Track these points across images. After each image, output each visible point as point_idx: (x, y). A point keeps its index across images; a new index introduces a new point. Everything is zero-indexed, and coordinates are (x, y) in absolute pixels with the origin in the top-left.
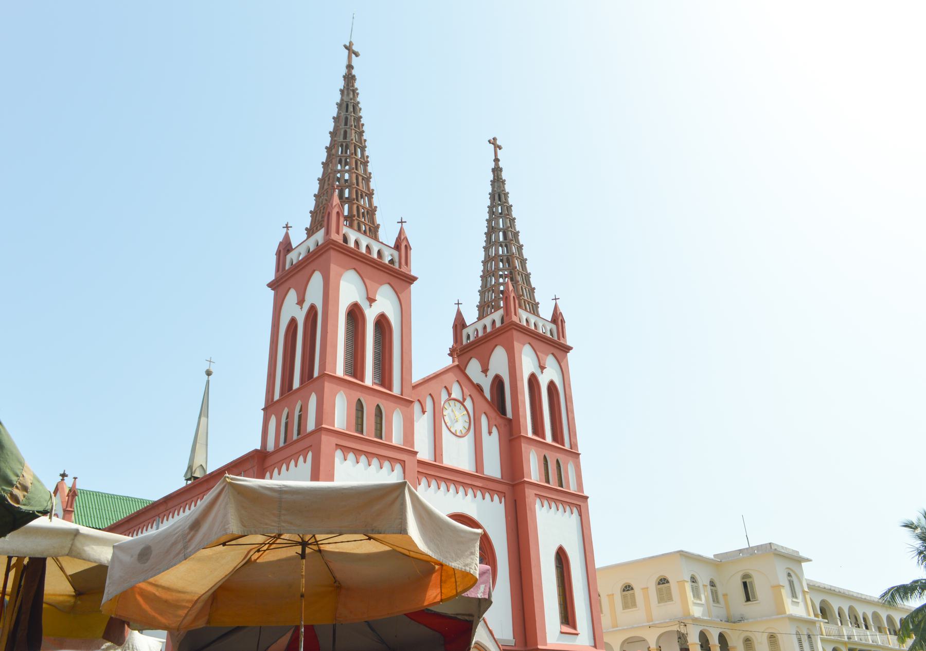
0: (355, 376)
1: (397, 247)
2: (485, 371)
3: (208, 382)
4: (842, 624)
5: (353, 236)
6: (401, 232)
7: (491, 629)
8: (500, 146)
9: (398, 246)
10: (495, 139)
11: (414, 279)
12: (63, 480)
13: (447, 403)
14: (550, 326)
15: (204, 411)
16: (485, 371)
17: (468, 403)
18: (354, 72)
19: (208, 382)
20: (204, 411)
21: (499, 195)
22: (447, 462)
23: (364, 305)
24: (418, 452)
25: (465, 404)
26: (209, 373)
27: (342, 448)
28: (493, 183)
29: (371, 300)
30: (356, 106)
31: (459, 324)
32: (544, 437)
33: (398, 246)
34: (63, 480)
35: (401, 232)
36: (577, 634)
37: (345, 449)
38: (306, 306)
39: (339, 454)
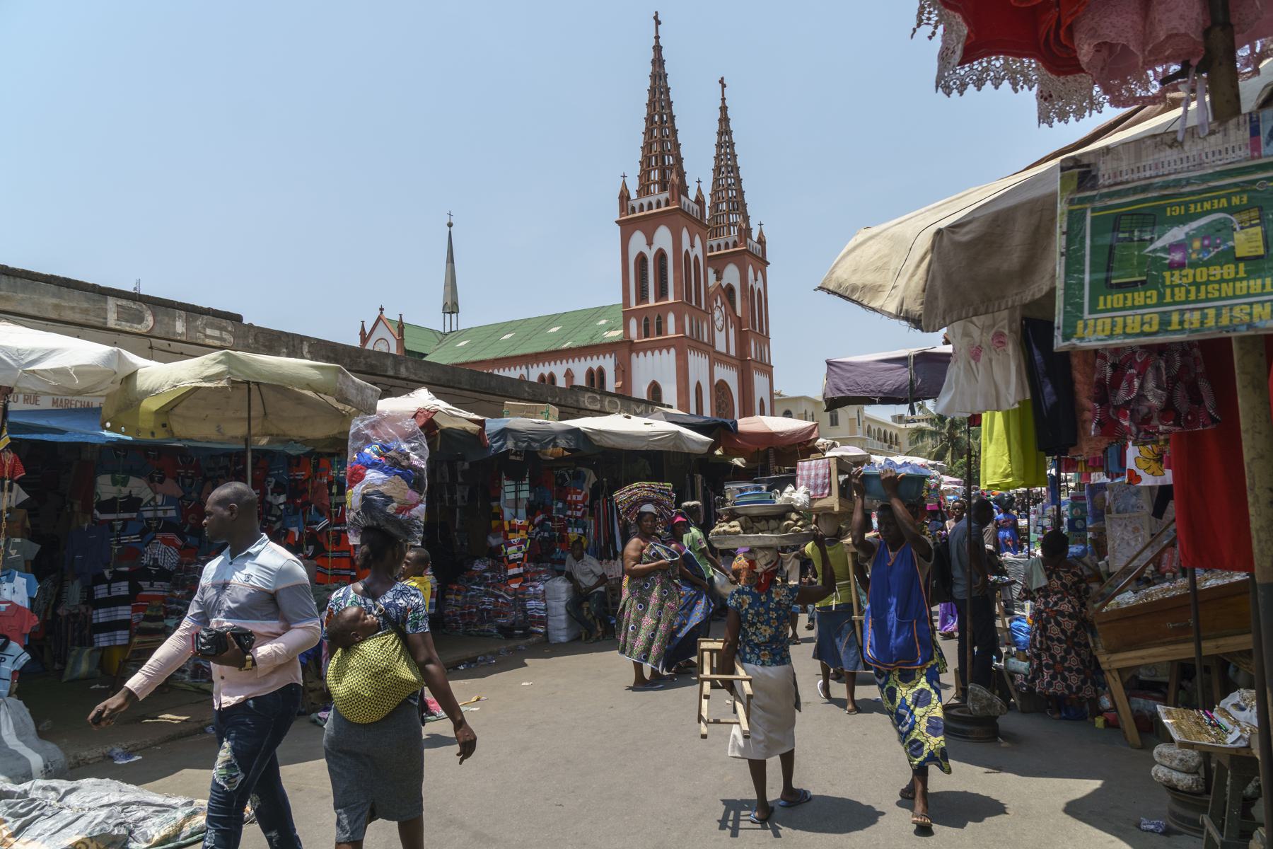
2: (650, 243)
3: (450, 232)
4: (318, 571)
10: (722, 79)
12: (382, 313)
14: (696, 207)
15: (451, 259)
16: (650, 243)
17: (723, 309)
18: (661, 44)
19: (450, 232)
20: (451, 259)
21: (658, 62)
26: (450, 225)
28: (720, 121)
30: (732, 145)
31: (624, 197)
32: (691, 302)
34: (382, 313)
38: (655, 248)
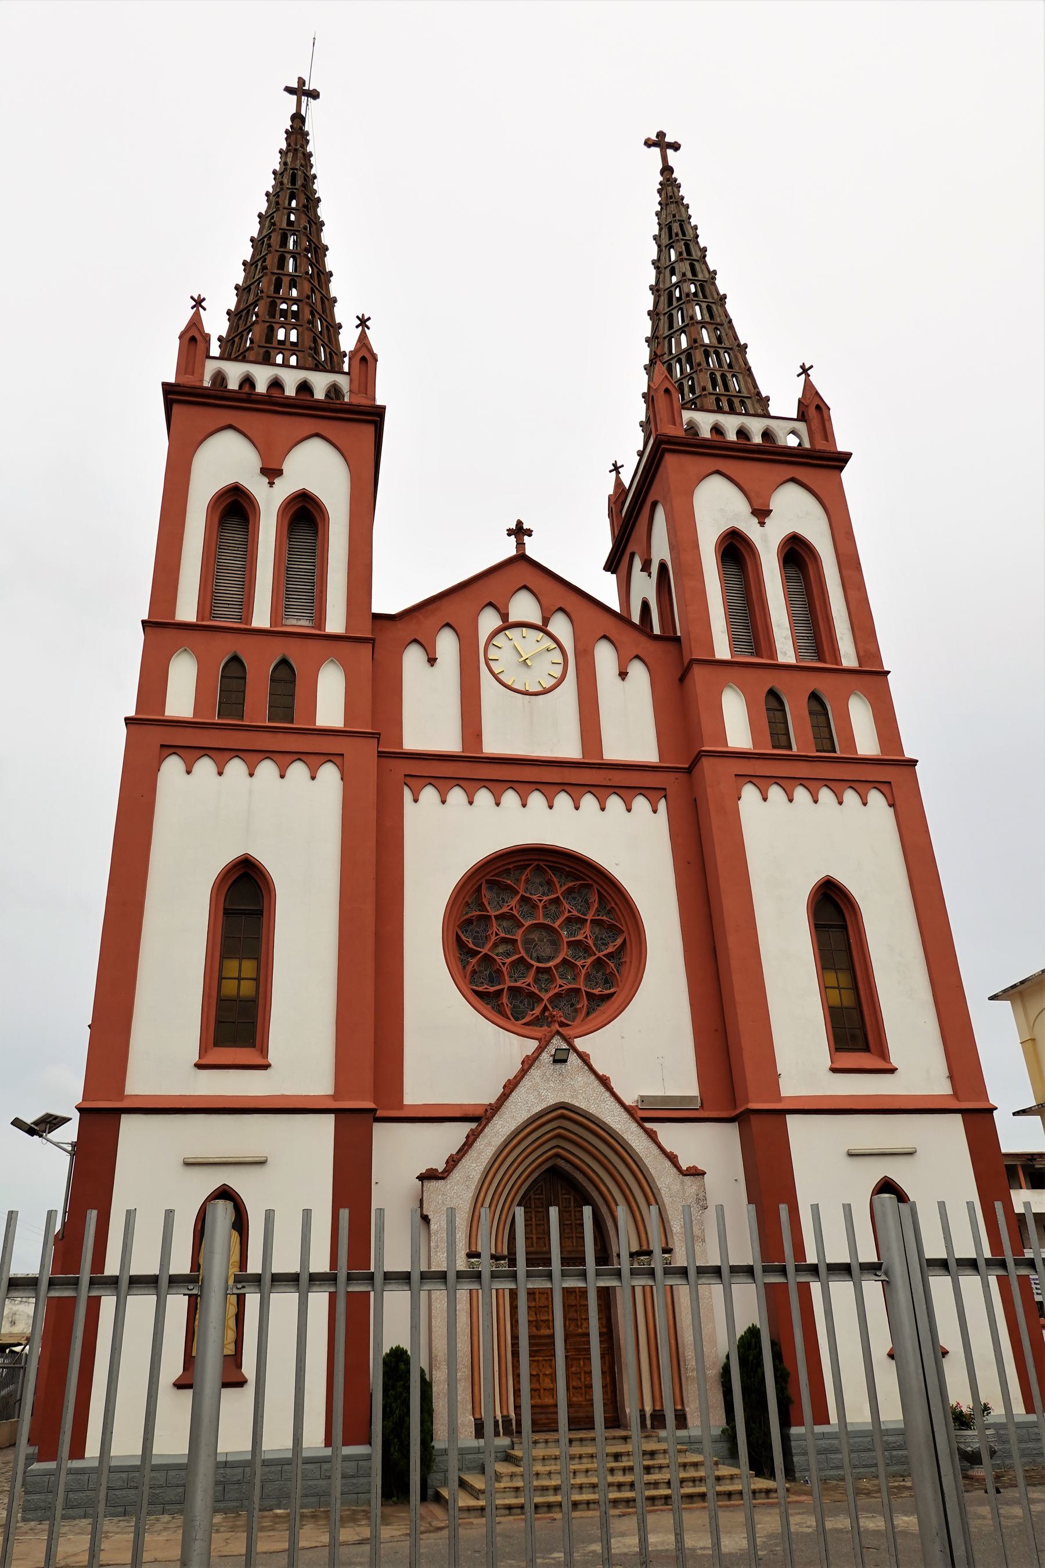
0: (758, 655)
1: (802, 416)
5: (291, 380)
6: (808, 387)
7: (601, 1073)
8: (676, 142)
9: (803, 413)
11: (844, 458)
13: (499, 640)
22: (612, 752)
23: (750, 528)
24: (917, 761)
25: (550, 628)
27: (805, 782)
29: (761, 514)
33: (803, 413)
35: (808, 387)
36: (266, 1067)
37: (762, 782)
39: (749, 793)
